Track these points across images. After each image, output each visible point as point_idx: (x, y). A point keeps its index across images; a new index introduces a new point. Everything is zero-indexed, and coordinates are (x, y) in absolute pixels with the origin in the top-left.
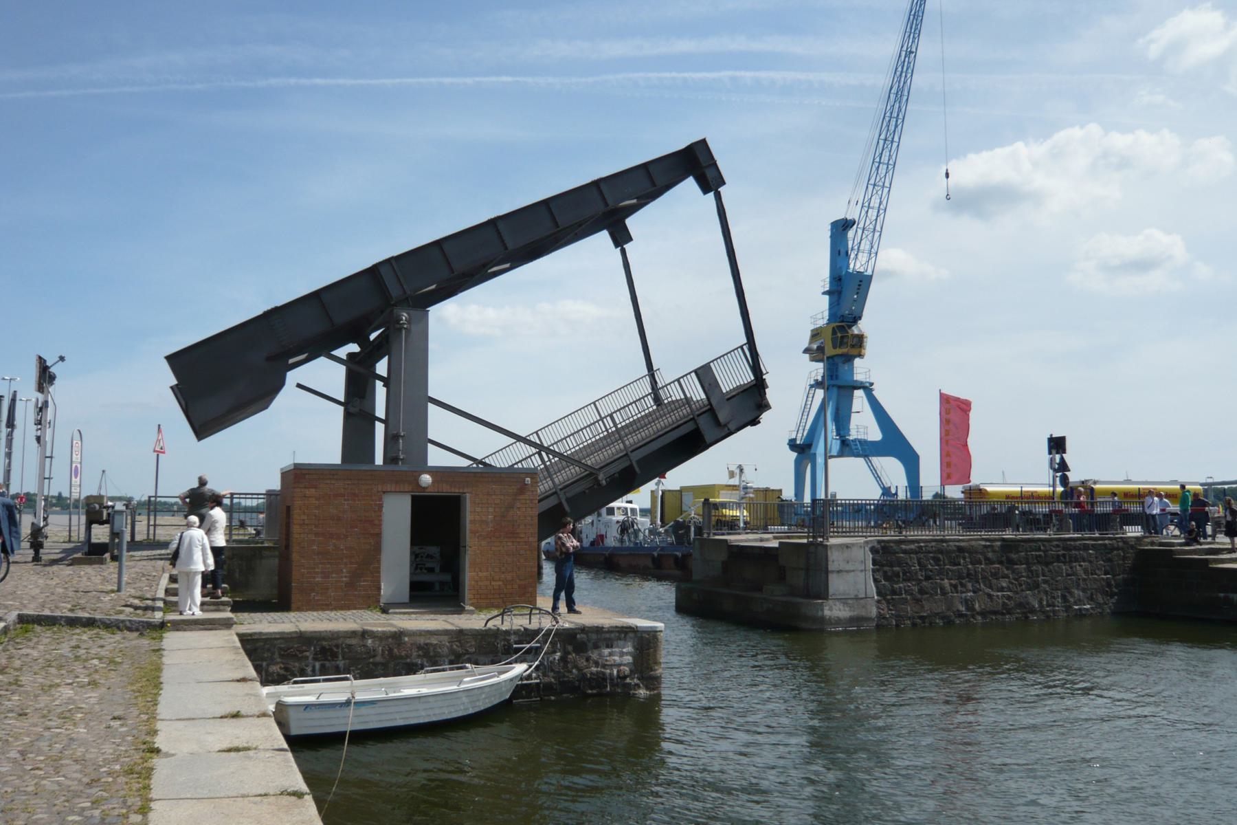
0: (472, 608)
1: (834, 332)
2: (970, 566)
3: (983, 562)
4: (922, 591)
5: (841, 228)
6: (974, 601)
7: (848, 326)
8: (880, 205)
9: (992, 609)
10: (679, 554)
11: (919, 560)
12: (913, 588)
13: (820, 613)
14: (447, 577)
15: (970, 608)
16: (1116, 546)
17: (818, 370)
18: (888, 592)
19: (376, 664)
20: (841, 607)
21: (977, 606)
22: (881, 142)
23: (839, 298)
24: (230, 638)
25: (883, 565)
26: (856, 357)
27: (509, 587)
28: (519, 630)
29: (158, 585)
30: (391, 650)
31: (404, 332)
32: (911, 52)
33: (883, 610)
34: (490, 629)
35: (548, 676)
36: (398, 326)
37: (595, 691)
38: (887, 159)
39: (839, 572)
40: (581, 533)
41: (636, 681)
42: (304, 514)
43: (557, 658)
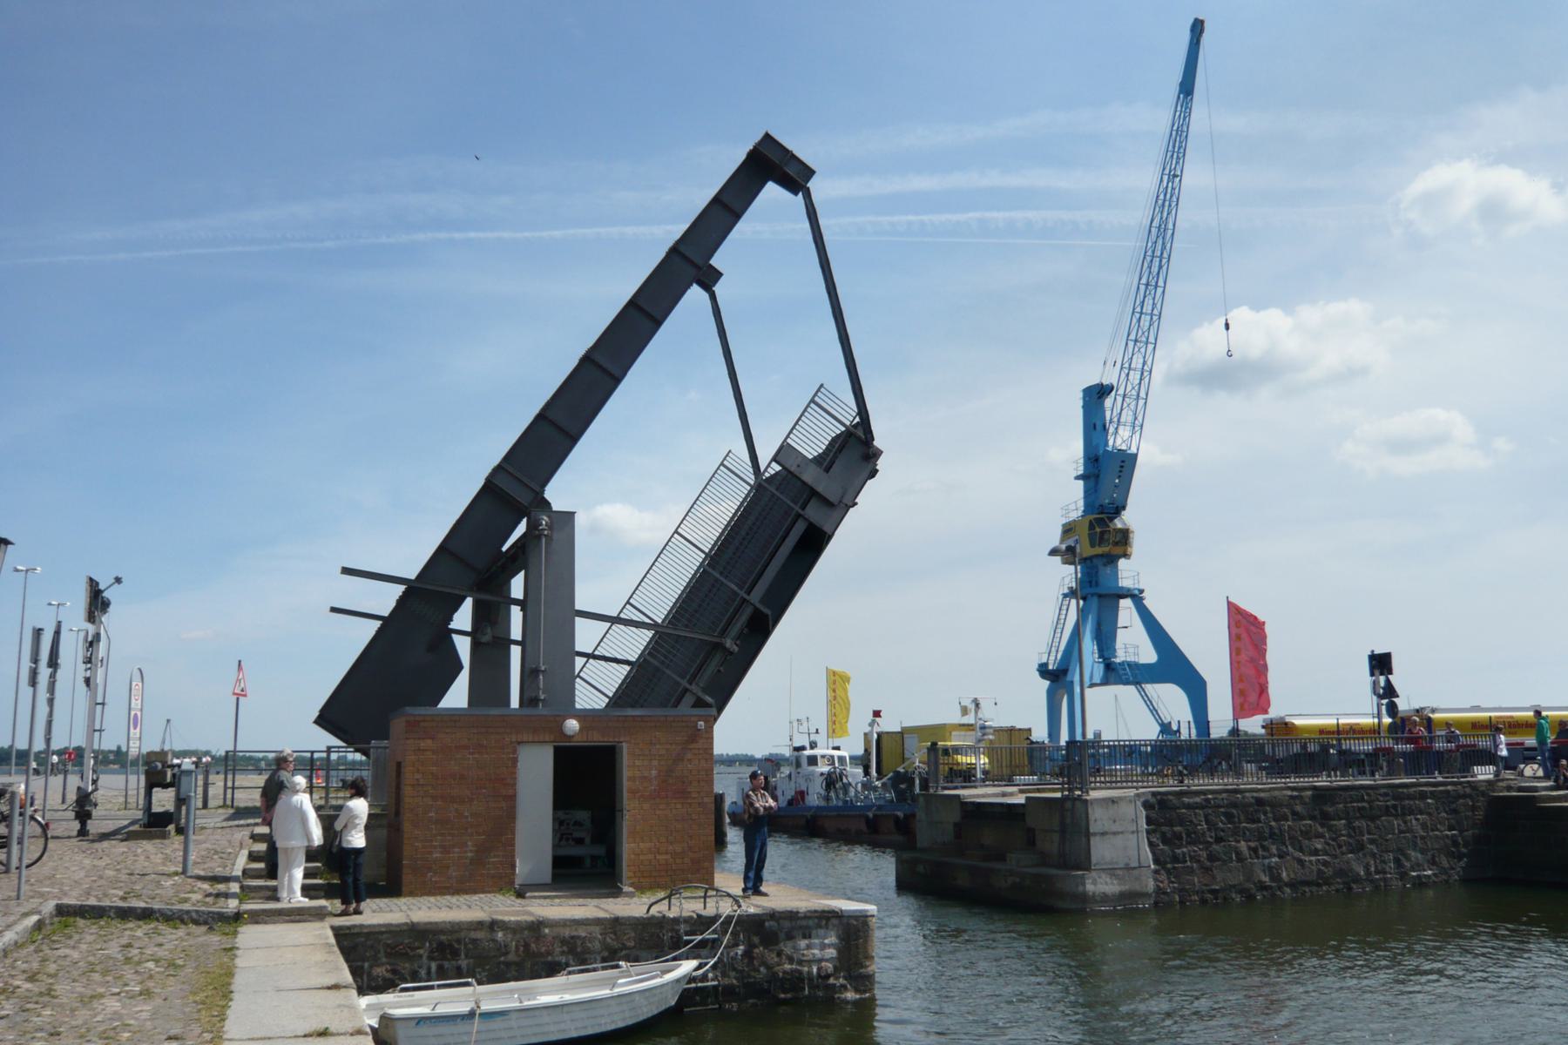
0: (631, 889)
1: (1091, 526)
2: (1273, 823)
5: (1096, 395)
6: (1281, 868)
7: (1109, 518)
11: (1206, 816)
13: (1081, 889)
14: (600, 850)
15: (1276, 877)
18: (1168, 860)
19: (508, 964)
20: (1108, 880)
21: (1284, 874)
22: (1142, 288)
23: (1097, 483)
24: (323, 932)
25: (1159, 825)
26: (1119, 557)
27: (678, 861)
28: (691, 917)
29: (233, 865)
30: (527, 946)
31: (544, 540)
33: (1162, 882)
34: (653, 917)
37: (789, 996)
38: (1150, 308)
39: (1103, 834)
42: (418, 771)
43: (740, 952)
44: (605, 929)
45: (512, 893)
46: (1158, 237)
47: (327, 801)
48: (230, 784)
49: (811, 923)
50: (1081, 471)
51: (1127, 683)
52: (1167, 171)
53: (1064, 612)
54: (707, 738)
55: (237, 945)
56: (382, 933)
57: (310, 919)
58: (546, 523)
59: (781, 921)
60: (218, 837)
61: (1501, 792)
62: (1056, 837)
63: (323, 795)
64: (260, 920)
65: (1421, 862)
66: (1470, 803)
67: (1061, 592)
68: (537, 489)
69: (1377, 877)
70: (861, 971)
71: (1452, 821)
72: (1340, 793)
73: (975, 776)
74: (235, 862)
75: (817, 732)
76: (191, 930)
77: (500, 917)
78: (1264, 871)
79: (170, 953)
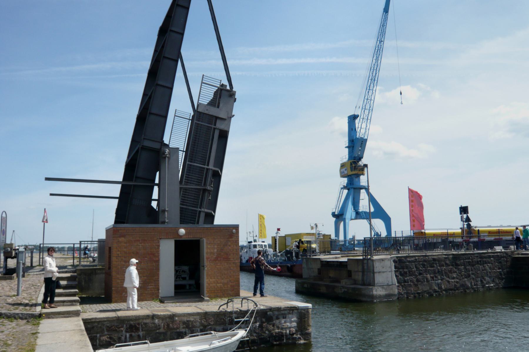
0: (208, 298)
1: (351, 164)
2: (439, 268)
3: (445, 265)
4: (418, 281)
5: (353, 119)
6: (442, 284)
7: (357, 161)
8: (370, 108)
9: (450, 288)
10: (289, 265)
11: (416, 265)
12: (414, 279)
13: (371, 293)
14: (192, 282)
15: (440, 288)
16: (503, 255)
17: (345, 181)
18: (402, 282)
19: (160, 333)
20: (381, 289)
21: (443, 287)
22: (370, 81)
23: (353, 149)
24: (77, 323)
25: (399, 269)
26: (361, 175)
27: (226, 286)
28: (237, 311)
29: (40, 291)
30: (168, 325)
31: (167, 159)
32: (382, 41)
33: (400, 290)
34: (221, 311)
35: (253, 336)
36: (164, 156)
37: (278, 343)
38: (372, 87)
39: (379, 272)
40: (242, 256)
41: (299, 336)
42: (118, 251)
43: (257, 325)
44: (201, 317)
45: (158, 301)
46: (375, 62)
47: (80, 263)
48: (41, 257)
49: (286, 312)
50: (347, 145)
51: (364, 219)
52: (379, 40)
53: (341, 194)
54: (236, 236)
55: (38, 331)
56: (106, 321)
57: (73, 316)
58: (168, 152)
59: (274, 312)
60: (34, 278)
61: (516, 255)
62: (361, 274)
63: (78, 260)
64: (51, 317)
65: (489, 281)
66: (506, 259)
67: (340, 187)
68: (161, 141)
69: (475, 287)
70: (307, 331)
71: (500, 266)
72: (462, 256)
73: (316, 251)
74: (40, 290)
75: (256, 236)
76: (19, 323)
77: (156, 313)
78: (436, 285)
79: (6, 337)
